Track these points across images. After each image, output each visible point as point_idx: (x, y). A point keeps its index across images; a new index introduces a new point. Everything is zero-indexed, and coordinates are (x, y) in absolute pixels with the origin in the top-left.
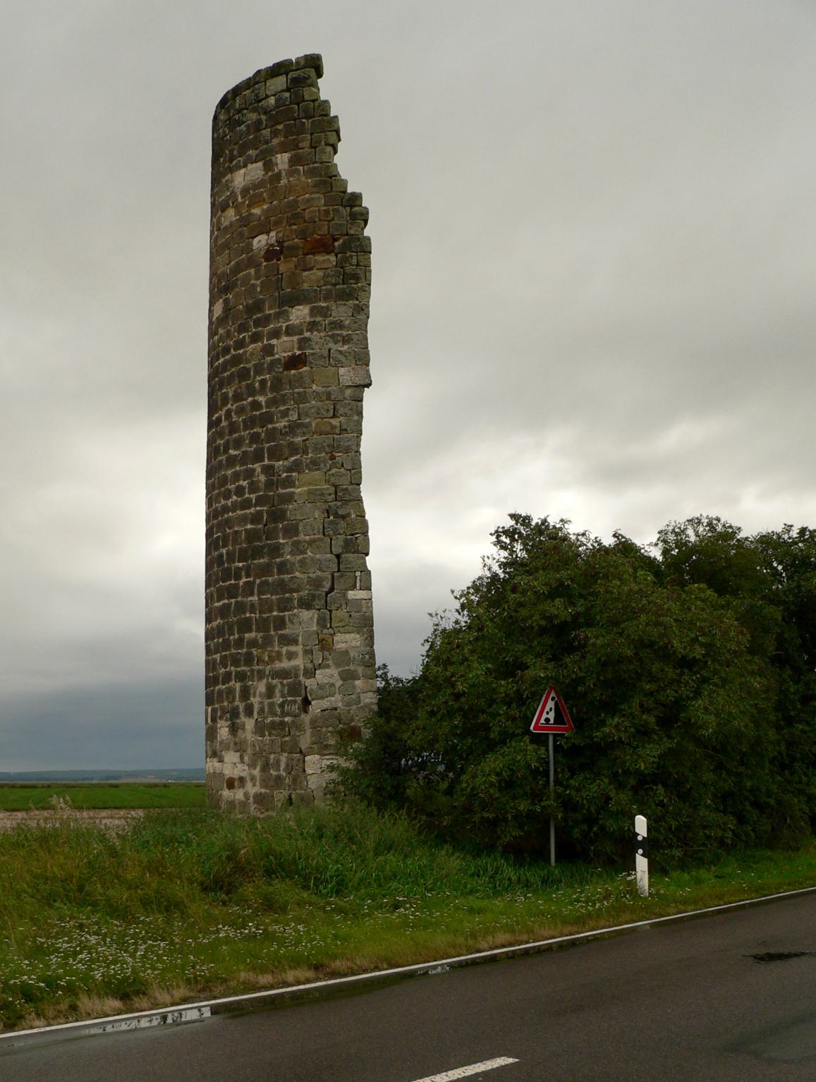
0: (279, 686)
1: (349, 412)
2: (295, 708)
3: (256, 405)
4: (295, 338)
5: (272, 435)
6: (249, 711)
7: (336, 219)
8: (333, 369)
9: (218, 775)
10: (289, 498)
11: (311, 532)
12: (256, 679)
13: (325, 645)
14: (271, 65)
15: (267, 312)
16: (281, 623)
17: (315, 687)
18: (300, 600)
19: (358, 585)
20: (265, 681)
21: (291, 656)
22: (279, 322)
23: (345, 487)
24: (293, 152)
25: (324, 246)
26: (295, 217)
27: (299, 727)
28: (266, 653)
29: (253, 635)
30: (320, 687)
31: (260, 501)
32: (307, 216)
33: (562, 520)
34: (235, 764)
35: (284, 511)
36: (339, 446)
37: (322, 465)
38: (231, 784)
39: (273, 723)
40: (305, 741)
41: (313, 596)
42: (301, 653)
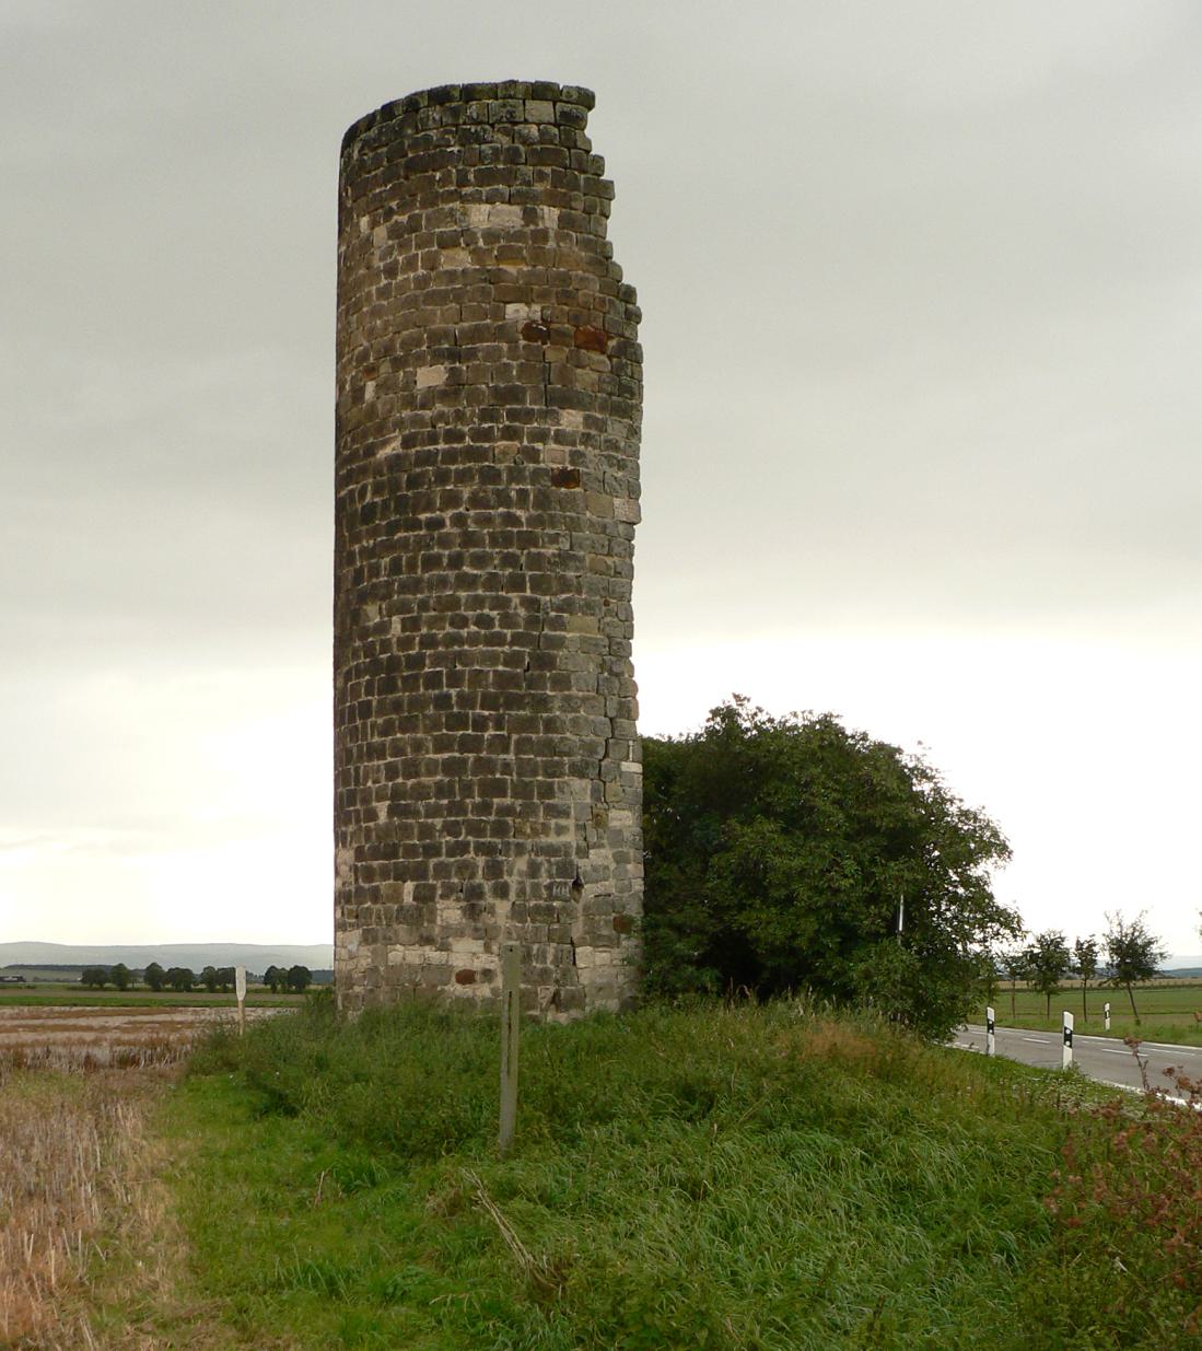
0: (546, 865)
1: (623, 553)
2: (566, 892)
3: (511, 519)
4: (567, 449)
5: (536, 561)
6: (502, 891)
7: (612, 312)
8: (608, 497)
9: (445, 968)
10: (559, 643)
11: (585, 688)
12: (512, 853)
13: (599, 821)
14: (534, 81)
15: (528, 406)
16: (547, 792)
17: (589, 868)
18: (572, 765)
19: (631, 756)
20: (526, 857)
21: (560, 830)
22: (546, 422)
23: (619, 640)
24: (564, 210)
25: (597, 342)
26: (566, 297)
27: (570, 914)
28: (528, 824)
29: (508, 801)
30: (595, 869)
31: (516, 639)
32: (581, 299)
33: (737, 697)
34: (474, 954)
35: (553, 658)
36: (614, 591)
37: (597, 610)
38: (466, 977)
39: (537, 907)
40: (577, 930)
41: (587, 764)
42: (572, 828)
